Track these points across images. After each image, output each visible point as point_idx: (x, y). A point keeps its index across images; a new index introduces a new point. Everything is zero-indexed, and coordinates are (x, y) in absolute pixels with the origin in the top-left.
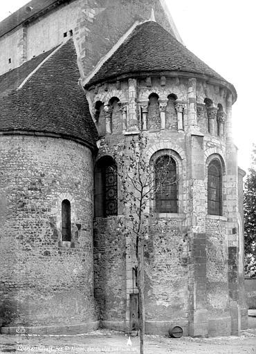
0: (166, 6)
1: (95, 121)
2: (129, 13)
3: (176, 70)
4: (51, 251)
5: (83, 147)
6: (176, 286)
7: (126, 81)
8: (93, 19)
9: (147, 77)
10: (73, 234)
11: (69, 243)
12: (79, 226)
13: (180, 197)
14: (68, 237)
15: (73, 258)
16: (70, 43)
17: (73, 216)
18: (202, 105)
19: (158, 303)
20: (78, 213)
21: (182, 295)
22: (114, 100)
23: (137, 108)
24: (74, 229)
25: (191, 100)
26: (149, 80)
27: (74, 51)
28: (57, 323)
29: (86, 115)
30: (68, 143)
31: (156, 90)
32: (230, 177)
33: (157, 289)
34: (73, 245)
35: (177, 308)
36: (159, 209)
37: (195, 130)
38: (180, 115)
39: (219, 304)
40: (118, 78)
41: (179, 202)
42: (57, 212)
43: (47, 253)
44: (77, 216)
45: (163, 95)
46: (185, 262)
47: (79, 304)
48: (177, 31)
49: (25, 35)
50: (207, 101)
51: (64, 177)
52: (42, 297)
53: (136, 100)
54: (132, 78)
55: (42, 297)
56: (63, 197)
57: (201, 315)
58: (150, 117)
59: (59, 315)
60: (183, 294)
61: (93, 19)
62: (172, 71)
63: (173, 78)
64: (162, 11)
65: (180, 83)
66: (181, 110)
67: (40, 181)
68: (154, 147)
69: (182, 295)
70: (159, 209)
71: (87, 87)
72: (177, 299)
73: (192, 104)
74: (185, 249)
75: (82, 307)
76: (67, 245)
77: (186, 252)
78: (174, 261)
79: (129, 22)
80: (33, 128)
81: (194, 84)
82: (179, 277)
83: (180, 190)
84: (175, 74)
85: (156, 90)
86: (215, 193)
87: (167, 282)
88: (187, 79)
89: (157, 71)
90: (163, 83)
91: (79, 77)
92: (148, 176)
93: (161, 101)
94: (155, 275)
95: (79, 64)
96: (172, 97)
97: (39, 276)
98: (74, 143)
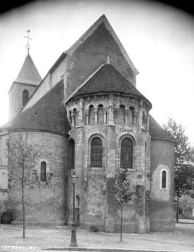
0: (125, 51)
1: (69, 121)
2: (97, 60)
3: (100, 92)
4: (34, 186)
5: (56, 135)
6: (99, 205)
7: (78, 100)
8: (73, 68)
9: (87, 97)
10: (47, 179)
11: (45, 183)
12: (51, 175)
13: (103, 159)
14: (45, 180)
15: (47, 190)
16: (63, 80)
17: (48, 169)
18: (118, 109)
19: (90, 213)
20: (50, 168)
21: (102, 210)
22: (75, 109)
23: (83, 113)
24: (48, 176)
25: (110, 107)
26: (88, 98)
27: (63, 85)
28: (36, 220)
29: (64, 118)
30: (45, 134)
31: (103, 103)
32: (138, 146)
33: (90, 207)
34: (47, 184)
35: (99, 216)
36: (92, 165)
37: (111, 123)
38: (105, 115)
39: (126, 216)
40: (75, 99)
41: (103, 162)
42: (38, 168)
43: (32, 187)
44: (51, 169)
45: (96, 106)
46: (104, 193)
47: (50, 212)
48: (133, 65)
49: (51, 78)
50: (122, 106)
51: (43, 151)
52: (29, 208)
53: (82, 109)
54: (81, 98)
55: (29, 208)
56: (42, 160)
57: (110, 221)
58: (91, 117)
59: (37, 217)
60: (102, 209)
61: (73, 68)
62: (117, 92)
63: (101, 96)
64: (122, 55)
65: (105, 98)
66: (105, 112)
67: (30, 153)
68: (90, 133)
69: (102, 210)
70: (92, 165)
71: (66, 104)
72: (99, 212)
73: (110, 109)
74: (105, 186)
75: (51, 214)
76: (43, 184)
77: (105, 188)
78: (98, 192)
79: (97, 65)
80: (26, 128)
81: (112, 98)
82: (101, 200)
83: (103, 155)
84: (100, 94)
85: (103, 103)
86: (128, 156)
87: (95, 203)
88: (108, 95)
89: (91, 93)
90: (95, 99)
91: (64, 99)
92: (88, 147)
93: (95, 109)
94: (89, 199)
95: (65, 92)
96: (101, 106)
97: (28, 198)
98: (49, 134)
